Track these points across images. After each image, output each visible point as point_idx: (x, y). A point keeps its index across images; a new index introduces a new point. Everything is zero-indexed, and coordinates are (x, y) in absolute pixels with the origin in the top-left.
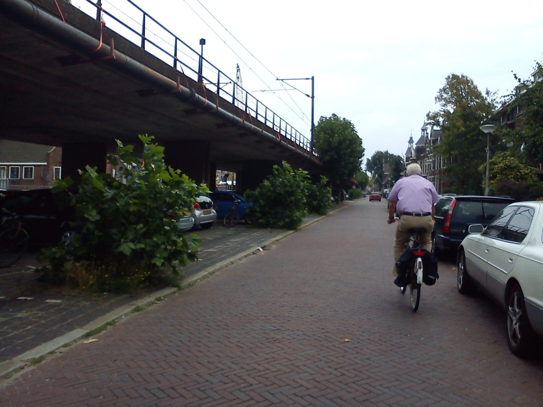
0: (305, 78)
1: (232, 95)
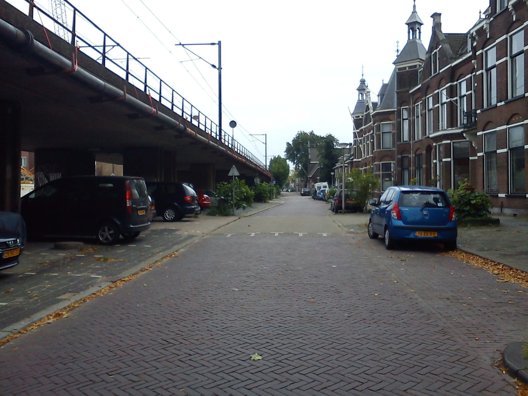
0: (210, 43)
1: (181, 109)
